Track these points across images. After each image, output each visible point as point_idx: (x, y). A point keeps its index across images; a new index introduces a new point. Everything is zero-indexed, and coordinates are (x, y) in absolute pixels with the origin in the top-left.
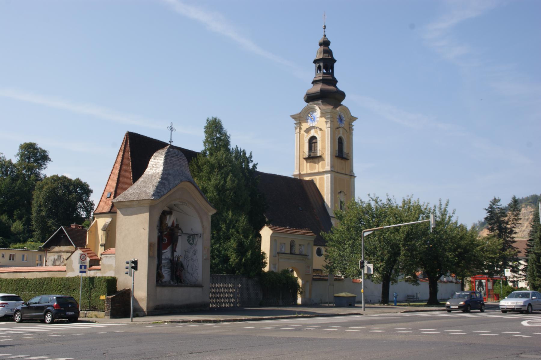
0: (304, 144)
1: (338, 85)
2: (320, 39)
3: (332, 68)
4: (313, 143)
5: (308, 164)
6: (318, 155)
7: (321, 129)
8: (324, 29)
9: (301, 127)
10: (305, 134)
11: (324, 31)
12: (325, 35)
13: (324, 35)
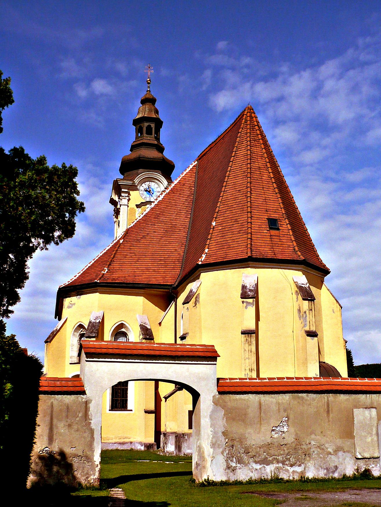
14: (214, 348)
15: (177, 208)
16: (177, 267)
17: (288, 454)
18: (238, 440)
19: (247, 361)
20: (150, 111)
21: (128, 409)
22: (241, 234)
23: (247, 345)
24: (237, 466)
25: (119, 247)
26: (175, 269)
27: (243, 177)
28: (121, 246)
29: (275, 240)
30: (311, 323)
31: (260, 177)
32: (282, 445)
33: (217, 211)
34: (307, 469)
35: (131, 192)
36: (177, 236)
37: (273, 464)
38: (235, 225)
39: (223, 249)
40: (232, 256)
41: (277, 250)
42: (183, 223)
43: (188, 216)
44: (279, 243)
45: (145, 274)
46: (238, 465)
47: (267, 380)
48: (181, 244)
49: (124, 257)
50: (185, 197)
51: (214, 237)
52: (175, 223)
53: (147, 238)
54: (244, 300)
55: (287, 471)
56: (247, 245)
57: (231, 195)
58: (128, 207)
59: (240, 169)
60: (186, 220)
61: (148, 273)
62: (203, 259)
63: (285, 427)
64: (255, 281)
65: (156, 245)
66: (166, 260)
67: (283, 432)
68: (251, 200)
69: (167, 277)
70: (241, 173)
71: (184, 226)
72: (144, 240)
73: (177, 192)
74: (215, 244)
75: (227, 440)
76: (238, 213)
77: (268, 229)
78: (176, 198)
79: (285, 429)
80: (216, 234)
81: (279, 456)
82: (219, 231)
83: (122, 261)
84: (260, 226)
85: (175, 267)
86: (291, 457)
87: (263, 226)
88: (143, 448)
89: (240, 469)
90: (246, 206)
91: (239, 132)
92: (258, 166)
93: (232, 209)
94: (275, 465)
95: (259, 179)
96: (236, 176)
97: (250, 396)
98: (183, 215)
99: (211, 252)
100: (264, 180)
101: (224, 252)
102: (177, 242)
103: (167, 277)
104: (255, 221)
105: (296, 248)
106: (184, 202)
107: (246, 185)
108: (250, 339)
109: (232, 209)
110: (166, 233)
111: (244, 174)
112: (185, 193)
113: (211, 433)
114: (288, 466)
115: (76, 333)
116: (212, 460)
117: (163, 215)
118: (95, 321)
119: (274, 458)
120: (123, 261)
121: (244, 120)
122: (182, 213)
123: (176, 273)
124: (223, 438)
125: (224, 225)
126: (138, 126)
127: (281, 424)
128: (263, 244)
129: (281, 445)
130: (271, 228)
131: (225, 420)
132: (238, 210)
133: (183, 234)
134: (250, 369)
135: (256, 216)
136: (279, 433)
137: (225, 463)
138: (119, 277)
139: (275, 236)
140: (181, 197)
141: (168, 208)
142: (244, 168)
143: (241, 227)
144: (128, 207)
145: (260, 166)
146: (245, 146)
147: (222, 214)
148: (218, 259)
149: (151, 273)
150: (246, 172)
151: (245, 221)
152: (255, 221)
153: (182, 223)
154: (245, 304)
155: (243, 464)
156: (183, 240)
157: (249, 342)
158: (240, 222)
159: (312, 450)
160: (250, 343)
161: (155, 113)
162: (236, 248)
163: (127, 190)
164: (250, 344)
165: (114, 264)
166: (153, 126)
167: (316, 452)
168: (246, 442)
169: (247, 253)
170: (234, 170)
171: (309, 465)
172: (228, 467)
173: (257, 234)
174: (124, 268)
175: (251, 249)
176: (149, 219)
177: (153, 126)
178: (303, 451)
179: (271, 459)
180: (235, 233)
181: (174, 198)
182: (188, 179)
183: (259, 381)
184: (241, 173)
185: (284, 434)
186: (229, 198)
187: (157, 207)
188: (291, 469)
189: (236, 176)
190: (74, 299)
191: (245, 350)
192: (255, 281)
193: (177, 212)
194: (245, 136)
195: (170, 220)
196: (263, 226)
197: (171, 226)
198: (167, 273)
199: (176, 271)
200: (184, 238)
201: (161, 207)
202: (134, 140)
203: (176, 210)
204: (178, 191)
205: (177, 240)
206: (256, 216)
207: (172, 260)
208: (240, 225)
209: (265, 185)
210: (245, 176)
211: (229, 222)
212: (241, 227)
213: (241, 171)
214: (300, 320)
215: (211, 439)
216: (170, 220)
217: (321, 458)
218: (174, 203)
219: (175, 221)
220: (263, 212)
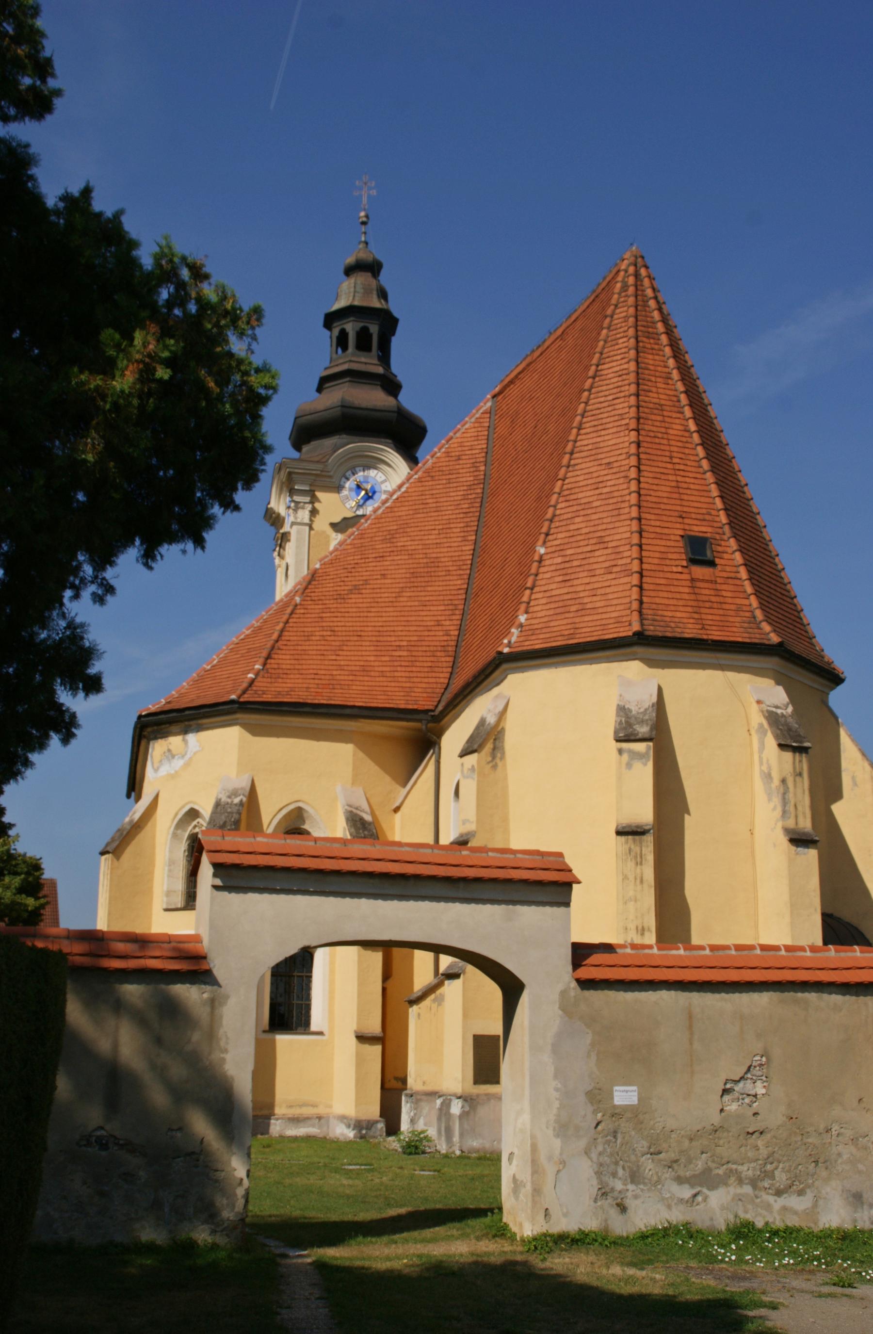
9: (317, 505)
14: (561, 859)
15: (440, 518)
16: (440, 664)
17: (768, 1158)
18: (629, 1115)
19: (631, 905)
20: (367, 291)
21: (314, 1027)
22: (613, 576)
23: (631, 864)
24: (627, 1190)
25: (292, 613)
26: (436, 670)
27: (619, 429)
28: (298, 611)
30: (800, 808)
31: (663, 430)
32: (752, 1134)
33: (549, 515)
34: (821, 1202)
35: (319, 494)
36: (440, 588)
37: (726, 1184)
38: (597, 553)
39: (567, 615)
40: (588, 633)
41: (710, 617)
42: (457, 554)
43: (470, 538)
45: (358, 683)
46: (631, 1187)
47: (707, 952)
48: (451, 607)
50: (462, 488)
51: (543, 582)
53: (364, 591)
54: (625, 745)
55: (768, 1207)
56: (631, 602)
57: (587, 477)
58: (311, 528)
59: (610, 409)
60: (464, 548)
61: (366, 678)
62: (514, 639)
63: (759, 1083)
64: (651, 696)
65: (387, 609)
66: (413, 649)
67: (755, 1096)
68: (639, 488)
69: (416, 690)
70: (612, 419)
71: (458, 563)
72: (357, 596)
73: (441, 478)
74: (544, 601)
75: (599, 1115)
76: (605, 521)
77: (685, 563)
78: (438, 491)
79: (760, 1089)
80: (548, 575)
81: (742, 1164)
82: (553, 568)
83: (300, 648)
84: (664, 556)
85: (437, 664)
86: (776, 1168)
87: (670, 556)
88: (351, 1134)
89: (636, 1197)
90: (626, 504)
91: (606, 317)
92: (656, 401)
93: (589, 512)
94: (733, 1190)
95: (660, 435)
96: (600, 428)
97: (665, 996)
98: (455, 535)
99: (533, 621)
100: (673, 438)
101: (569, 621)
102: (442, 603)
103: (416, 690)
104: (650, 541)
105: (759, 614)
107: (626, 450)
109: (589, 512)
110: (412, 580)
111: (619, 423)
112: (461, 480)
113: (556, 1094)
114: (768, 1194)
115: (179, 832)
116: (558, 1171)
118: (229, 800)
119: (731, 1170)
120: (304, 648)
121: (619, 285)
122: (454, 530)
123: (438, 680)
124: (590, 1108)
125: (569, 552)
126: (336, 332)
127: (749, 1076)
128: (671, 602)
129: (748, 1133)
130: (693, 561)
131: (594, 1057)
132: (605, 515)
133: (455, 583)
134: (640, 928)
135: (651, 529)
136: (743, 1099)
137: (595, 1182)
138: (292, 689)
139: (703, 581)
140: (452, 490)
141: (419, 516)
142: (621, 406)
143: (613, 556)
144: (311, 528)
145: (663, 402)
146: (623, 350)
147: (561, 524)
148: (552, 639)
149: (373, 679)
150: (625, 416)
151: (623, 542)
152: (650, 541)
153: (453, 554)
154: (625, 757)
155: (645, 1184)
156: (456, 597)
157: (636, 857)
158: (610, 545)
159: (834, 1150)
160: (639, 860)
161: (378, 297)
162: (600, 610)
163: (307, 488)
164: (639, 861)
165: (281, 657)
166: (374, 329)
167: (845, 1157)
168: (652, 1123)
169: (630, 625)
170: (594, 412)
171: (827, 1193)
172: (604, 1193)
173: (658, 574)
174: (304, 667)
175: (640, 612)
177: (374, 329)
178: (809, 1151)
179: (720, 1172)
180: (598, 572)
181: (434, 492)
182: (469, 444)
183: (688, 953)
184: (612, 419)
185: (757, 1104)
186: (581, 484)
187: (390, 515)
188: (778, 1203)
189: (600, 428)
190: (175, 741)
191: (625, 878)
192: (651, 696)
193: (441, 527)
194: (623, 324)
196: (670, 556)
197: (425, 561)
198: (415, 680)
199: (437, 675)
200: (460, 592)
202: (327, 364)
203: (437, 523)
205: (441, 598)
206: (651, 529)
207: (427, 649)
208: (609, 551)
209: (675, 449)
210: (623, 428)
211: (582, 543)
212: (613, 556)
213: (613, 413)
214: (770, 800)
215: (555, 1111)
217: (860, 1172)
218: (434, 505)
219: (435, 551)
220: (671, 519)
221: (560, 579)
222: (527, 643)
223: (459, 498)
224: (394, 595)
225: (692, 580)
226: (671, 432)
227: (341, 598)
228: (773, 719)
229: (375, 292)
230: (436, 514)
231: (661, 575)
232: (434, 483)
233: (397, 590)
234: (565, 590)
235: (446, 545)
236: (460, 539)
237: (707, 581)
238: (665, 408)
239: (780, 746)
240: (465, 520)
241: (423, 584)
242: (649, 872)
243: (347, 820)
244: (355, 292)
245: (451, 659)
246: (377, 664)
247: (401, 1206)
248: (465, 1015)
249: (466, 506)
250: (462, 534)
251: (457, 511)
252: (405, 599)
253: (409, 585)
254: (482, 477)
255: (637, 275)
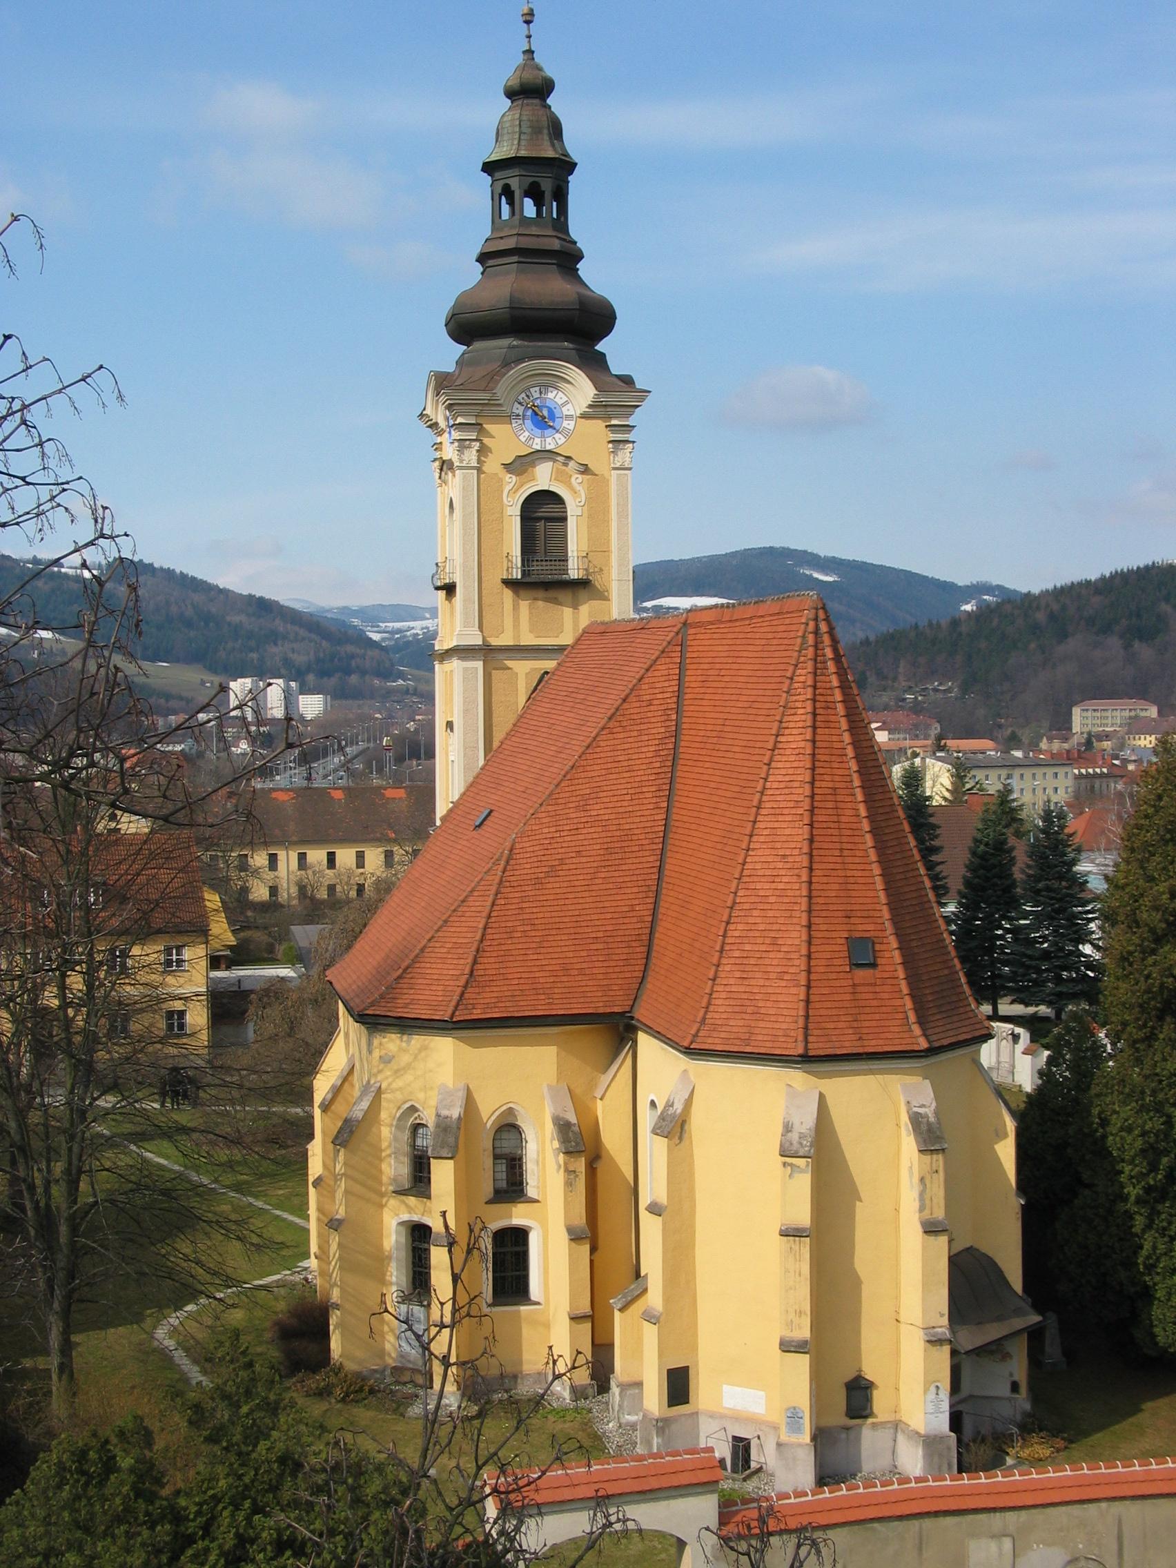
0: (501, 520)
1: (583, 268)
2: (507, 70)
3: (561, 195)
4: (539, 519)
5: (524, 605)
6: (574, 574)
7: (585, 470)
8: (528, 22)
9: (486, 440)
10: (510, 480)
11: (526, 33)
12: (529, 52)
13: (524, 52)
29: (864, 996)
30: (935, 1201)
38: (771, 955)
44: (875, 1003)
48: (644, 889)
49: (508, 935)
52: (627, 827)
53: (561, 873)
59: (786, 791)
71: (651, 836)
106: (651, 760)
108: (797, 1248)
117: (598, 800)
125: (747, 947)
139: (863, 985)
144: (479, 470)
176: (564, 812)
191: (787, 1271)
195: (617, 816)
201: (593, 774)
204: (636, 722)
205: (635, 878)
216: (617, 816)
221: (738, 975)
222: (710, 1040)
223: (650, 755)
224: (589, 877)
225: (854, 985)
226: (843, 819)
227: (538, 882)
228: (917, 1121)
229: (545, 131)
230: (628, 774)
231: (826, 983)
232: (626, 735)
233: (592, 871)
234: (742, 989)
235: (639, 813)
236: (651, 806)
237: (868, 985)
238: (838, 791)
239: (920, 1151)
240: (658, 782)
241: (617, 862)
242: (806, 1268)
243: (555, 1124)
244: (521, 133)
245: (645, 949)
246: (575, 960)
247: (603, 1118)
248: (660, 1356)
249: (658, 765)
250: (654, 800)
251: (649, 771)
252: (600, 881)
253: (603, 864)
254: (674, 728)
255: (816, 632)
